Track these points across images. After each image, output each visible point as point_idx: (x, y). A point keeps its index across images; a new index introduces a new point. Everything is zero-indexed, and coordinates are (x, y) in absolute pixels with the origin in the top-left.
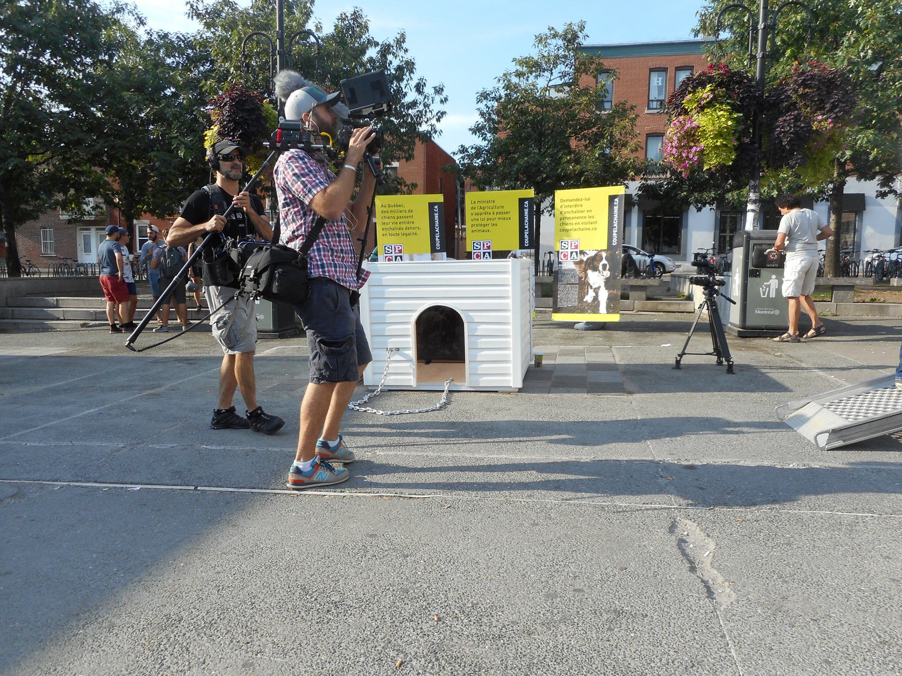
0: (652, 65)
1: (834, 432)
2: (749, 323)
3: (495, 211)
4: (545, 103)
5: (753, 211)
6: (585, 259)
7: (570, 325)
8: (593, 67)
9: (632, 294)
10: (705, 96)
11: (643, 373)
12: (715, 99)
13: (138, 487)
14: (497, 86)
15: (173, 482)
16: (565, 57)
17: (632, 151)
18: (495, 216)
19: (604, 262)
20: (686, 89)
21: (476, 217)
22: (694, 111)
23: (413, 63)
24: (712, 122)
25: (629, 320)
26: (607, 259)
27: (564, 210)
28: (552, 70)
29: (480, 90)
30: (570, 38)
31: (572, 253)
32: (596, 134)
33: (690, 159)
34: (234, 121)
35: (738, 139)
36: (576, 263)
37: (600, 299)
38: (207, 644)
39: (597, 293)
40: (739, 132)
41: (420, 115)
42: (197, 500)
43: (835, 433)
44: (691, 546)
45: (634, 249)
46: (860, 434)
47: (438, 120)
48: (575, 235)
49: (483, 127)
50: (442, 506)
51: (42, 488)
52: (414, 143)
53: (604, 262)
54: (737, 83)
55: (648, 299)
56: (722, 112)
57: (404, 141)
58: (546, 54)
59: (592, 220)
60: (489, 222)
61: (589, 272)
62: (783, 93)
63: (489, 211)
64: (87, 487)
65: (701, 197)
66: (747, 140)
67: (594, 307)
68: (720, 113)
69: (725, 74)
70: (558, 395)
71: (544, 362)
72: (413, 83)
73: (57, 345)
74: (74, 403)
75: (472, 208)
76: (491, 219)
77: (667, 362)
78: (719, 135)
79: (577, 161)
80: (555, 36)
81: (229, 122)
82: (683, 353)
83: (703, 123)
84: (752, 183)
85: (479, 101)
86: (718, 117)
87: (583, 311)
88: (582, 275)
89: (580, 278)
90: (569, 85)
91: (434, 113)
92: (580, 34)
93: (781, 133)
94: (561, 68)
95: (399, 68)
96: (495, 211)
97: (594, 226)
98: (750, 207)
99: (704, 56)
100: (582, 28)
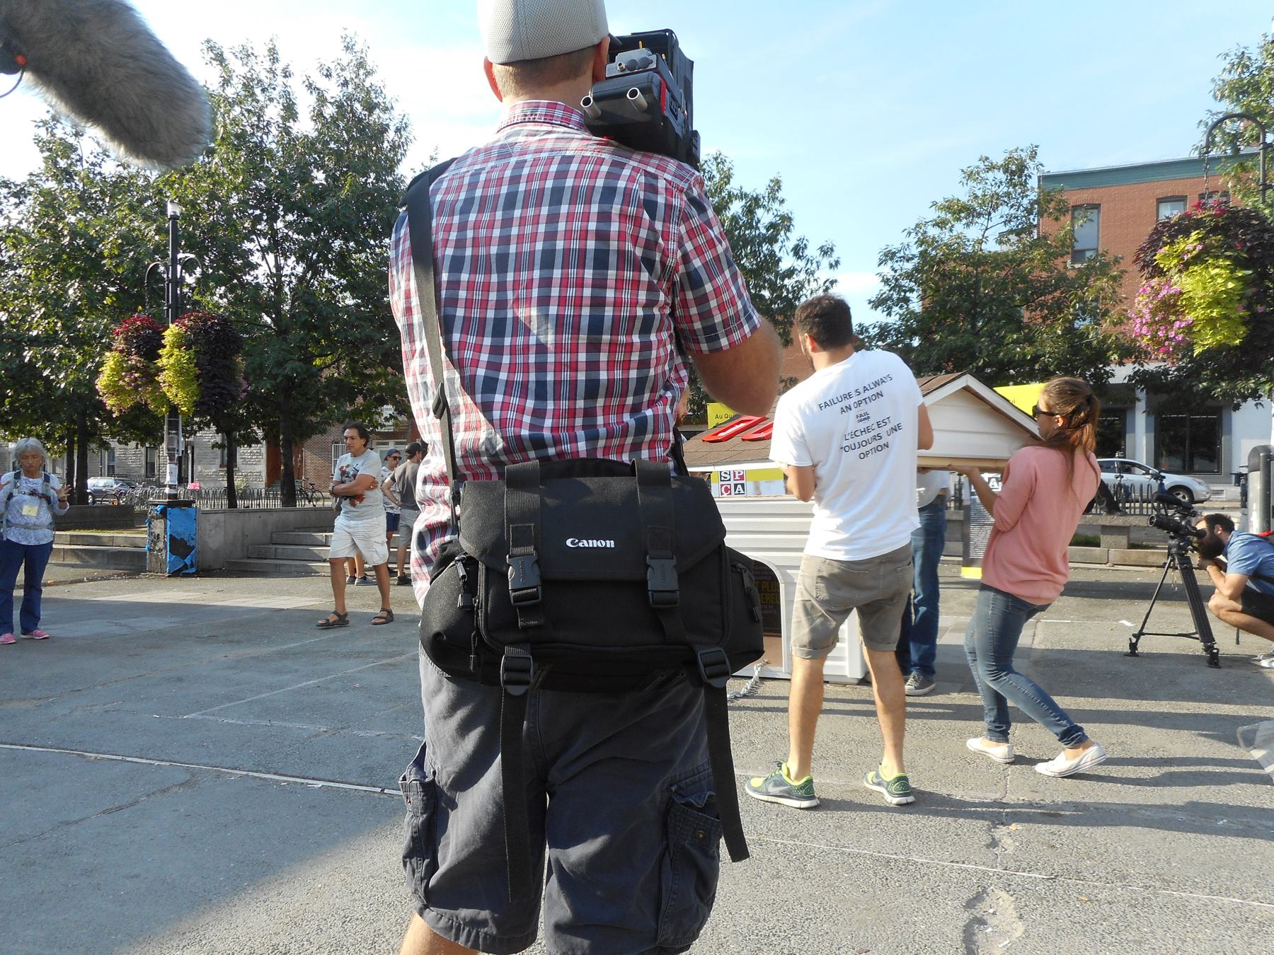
0: (1160, 193)
4: (978, 260)
8: (1052, 205)
9: (1105, 539)
10: (1190, 247)
11: (1066, 664)
12: (1206, 251)
13: (320, 784)
14: (906, 241)
15: (359, 781)
16: (1008, 194)
17: (1115, 324)
20: (1159, 239)
22: (1174, 271)
24: (1204, 285)
25: (1093, 580)
30: (1016, 170)
31: (736, 486)
32: (1059, 298)
33: (1171, 340)
35: (1248, 307)
40: (1254, 293)
41: (800, 286)
42: (375, 806)
44: (989, 930)
45: (1140, 467)
49: (890, 298)
51: (218, 777)
54: (1241, 226)
56: (1217, 270)
58: (979, 193)
64: (265, 779)
65: (1235, 387)
66: (1260, 309)
68: (1214, 272)
72: (790, 245)
73: (313, 594)
74: (297, 671)
77: (1114, 649)
78: (1216, 302)
79: (1030, 340)
80: (992, 168)
82: (1141, 633)
86: (1212, 277)
91: (821, 282)
92: (1031, 164)
94: (1004, 210)
95: (772, 226)
100: (1033, 155)
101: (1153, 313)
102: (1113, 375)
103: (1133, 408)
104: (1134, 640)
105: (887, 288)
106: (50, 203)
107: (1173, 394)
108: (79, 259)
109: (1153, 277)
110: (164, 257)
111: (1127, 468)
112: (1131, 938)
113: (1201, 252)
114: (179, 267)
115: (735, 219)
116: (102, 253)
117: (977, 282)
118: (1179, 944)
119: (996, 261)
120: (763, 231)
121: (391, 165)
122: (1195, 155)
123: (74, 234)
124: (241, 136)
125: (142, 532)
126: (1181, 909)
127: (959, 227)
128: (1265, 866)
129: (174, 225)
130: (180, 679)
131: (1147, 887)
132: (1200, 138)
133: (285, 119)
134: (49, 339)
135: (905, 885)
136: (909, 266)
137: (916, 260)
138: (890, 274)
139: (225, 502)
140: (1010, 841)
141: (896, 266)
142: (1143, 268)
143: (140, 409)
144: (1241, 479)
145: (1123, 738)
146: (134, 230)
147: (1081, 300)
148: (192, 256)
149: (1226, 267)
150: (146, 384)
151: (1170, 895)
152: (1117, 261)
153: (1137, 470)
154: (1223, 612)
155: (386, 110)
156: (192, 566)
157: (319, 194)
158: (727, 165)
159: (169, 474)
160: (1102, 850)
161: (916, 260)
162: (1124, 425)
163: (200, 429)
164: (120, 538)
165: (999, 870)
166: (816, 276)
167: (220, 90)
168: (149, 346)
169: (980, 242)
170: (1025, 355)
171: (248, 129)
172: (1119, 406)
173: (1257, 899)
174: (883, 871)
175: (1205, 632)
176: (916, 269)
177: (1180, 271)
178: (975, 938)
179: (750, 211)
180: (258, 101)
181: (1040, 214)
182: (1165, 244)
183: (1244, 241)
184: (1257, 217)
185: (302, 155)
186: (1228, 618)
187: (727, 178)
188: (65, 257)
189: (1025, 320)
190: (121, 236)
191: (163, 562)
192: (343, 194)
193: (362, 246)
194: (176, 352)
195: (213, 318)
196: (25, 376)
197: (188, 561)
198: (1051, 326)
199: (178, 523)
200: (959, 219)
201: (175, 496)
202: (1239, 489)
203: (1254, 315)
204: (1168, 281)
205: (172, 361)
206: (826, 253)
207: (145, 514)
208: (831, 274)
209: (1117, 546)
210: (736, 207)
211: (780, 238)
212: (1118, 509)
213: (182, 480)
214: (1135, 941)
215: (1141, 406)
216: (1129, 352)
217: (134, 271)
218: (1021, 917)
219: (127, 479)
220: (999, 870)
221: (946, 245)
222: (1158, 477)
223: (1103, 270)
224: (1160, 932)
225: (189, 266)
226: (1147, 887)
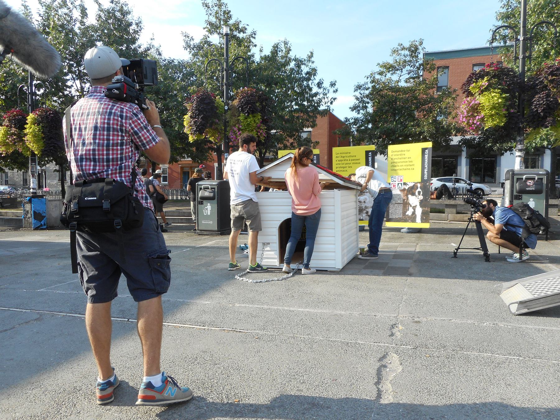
0: (474, 62)
1: (521, 303)
3: (351, 158)
4: (397, 90)
5: (519, 156)
6: (407, 188)
7: (398, 230)
8: (428, 66)
9: (447, 210)
10: (483, 84)
14: (366, 81)
15: (118, 316)
16: (410, 61)
19: (419, 190)
20: (471, 80)
21: (339, 162)
22: (477, 94)
23: (316, 70)
24: (489, 100)
25: (441, 227)
26: (421, 188)
27: (394, 157)
28: (402, 69)
29: (356, 84)
30: (414, 50)
34: (199, 110)
35: (507, 110)
36: (401, 191)
37: (416, 213)
38: (86, 403)
39: (414, 210)
40: (509, 104)
41: (320, 100)
43: (522, 303)
46: (540, 305)
47: (331, 103)
48: (400, 173)
49: (359, 106)
50: (254, 337)
51: (53, 316)
52: (316, 117)
53: (419, 190)
54: (505, 75)
55: (458, 213)
57: (309, 116)
59: (411, 164)
60: (347, 165)
61: (410, 196)
62: (537, 80)
63: (347, 158)
64: (72, 316)
65: (502, 146)
66: (512, 111)
67: (413, 219)
69: (496, 70)
72: (316, 82)
75: (337, 157)
76: (348, 164)
78: (493, 108)
79: (418, 126)
80: (403, 49)
81: (196, 110)
82: (459, 248)
83: (483, 101)
84: (518, 138)
86: (492, 97)
87: (405, 221)
88: (405, 198)
89: (404, 200)
90: (414, 78)
91: (329, 99)
92: (420, 47)
93: (537, 105)
94: (408, 68)
95: (308, 73)
96: (351, 158)
97: (412, 167)
99: (499, 56)
100: (421, 43)
101: (468, 112)
102: (452, 140)
103: (461, 155)
104: (456, 251)
107: (477, 149)
109: (468, 97)
110: (27, 82)
111: (457, 181)
112: (446, 371)
114: (34, 88)
115: (292, 69)
117: (396, 99)
118: (465, 373)
119: (404, 90)
120: (304, 76)
121: (134, 41)
125: (21, 210)
126: (467, 359)
127: (389, 75)
128: (502, 341)
130: (37, 274)
131: (454, 350)
132: (489, 36)
133: (83, 17)
135: (354, 353)
136: (367, 92)
137: (370, 89)
138: (359, 96)
139: (61, 197)
140: (399, 334)
142: (464, 93)
143: (16, 153)
144: (503, 184)
145: (448, 291)
146: (12, 70)
147: (440, 108)
149: (498, 93)
150: (19, 142)
151: (463, 353)
152: (455, 91)
153: (462, 182)
154: (492, 238)
156: (44, 225)
158: (289, 45)
159: (33, 183)
160: (437, 335)
161: (370, 89)
162: (457, 163)
163: (48, 163)
164: (10, 213)
165: (394, 345)
166: (328, 96)
168: (20, 124)
169: (398, 82)
170: (416, 132)
171: (65, 22)
172: (454, 154)
173: (498, 354)
174: (345, 347)
175: (484, 246)
176: (370, 94)
177: (480, 94)
178: (382, 373)
179: (299, 66)
181: (423, 70)
182: (474, 82)
183: (506, 81)
184: (512, 71)
186: (495, 241)
187: (289, 51)
189: (416, 116)
190: (5, 72)
191: (31, 223)
194: (33, 126)
195: (50, 111)
197: (42, 223)
198: (427, 119)
199: (37, 205)
200: (389, 72)
201: (36, 193)
202: (503, 189)
203: (509, 113)
204: (475, 98)
205: (31, 130)
207: (21, 201)
208: (334, 95)
209: (452, 213)
210: (292, 64)
211: (312, 78)
212: (453, 197)
213: (40, 186)
214: (447, 372)
215: (464, 154)
216: (460, 131)
217: (12, 89)
218: (401, 364)
219: (14, 186)
220: (394, 345)
221: (383, 82)
222: (469, 184)
223: (449, 95)
224: (457, 368)
225: (38, 87)
226: (454, 350)
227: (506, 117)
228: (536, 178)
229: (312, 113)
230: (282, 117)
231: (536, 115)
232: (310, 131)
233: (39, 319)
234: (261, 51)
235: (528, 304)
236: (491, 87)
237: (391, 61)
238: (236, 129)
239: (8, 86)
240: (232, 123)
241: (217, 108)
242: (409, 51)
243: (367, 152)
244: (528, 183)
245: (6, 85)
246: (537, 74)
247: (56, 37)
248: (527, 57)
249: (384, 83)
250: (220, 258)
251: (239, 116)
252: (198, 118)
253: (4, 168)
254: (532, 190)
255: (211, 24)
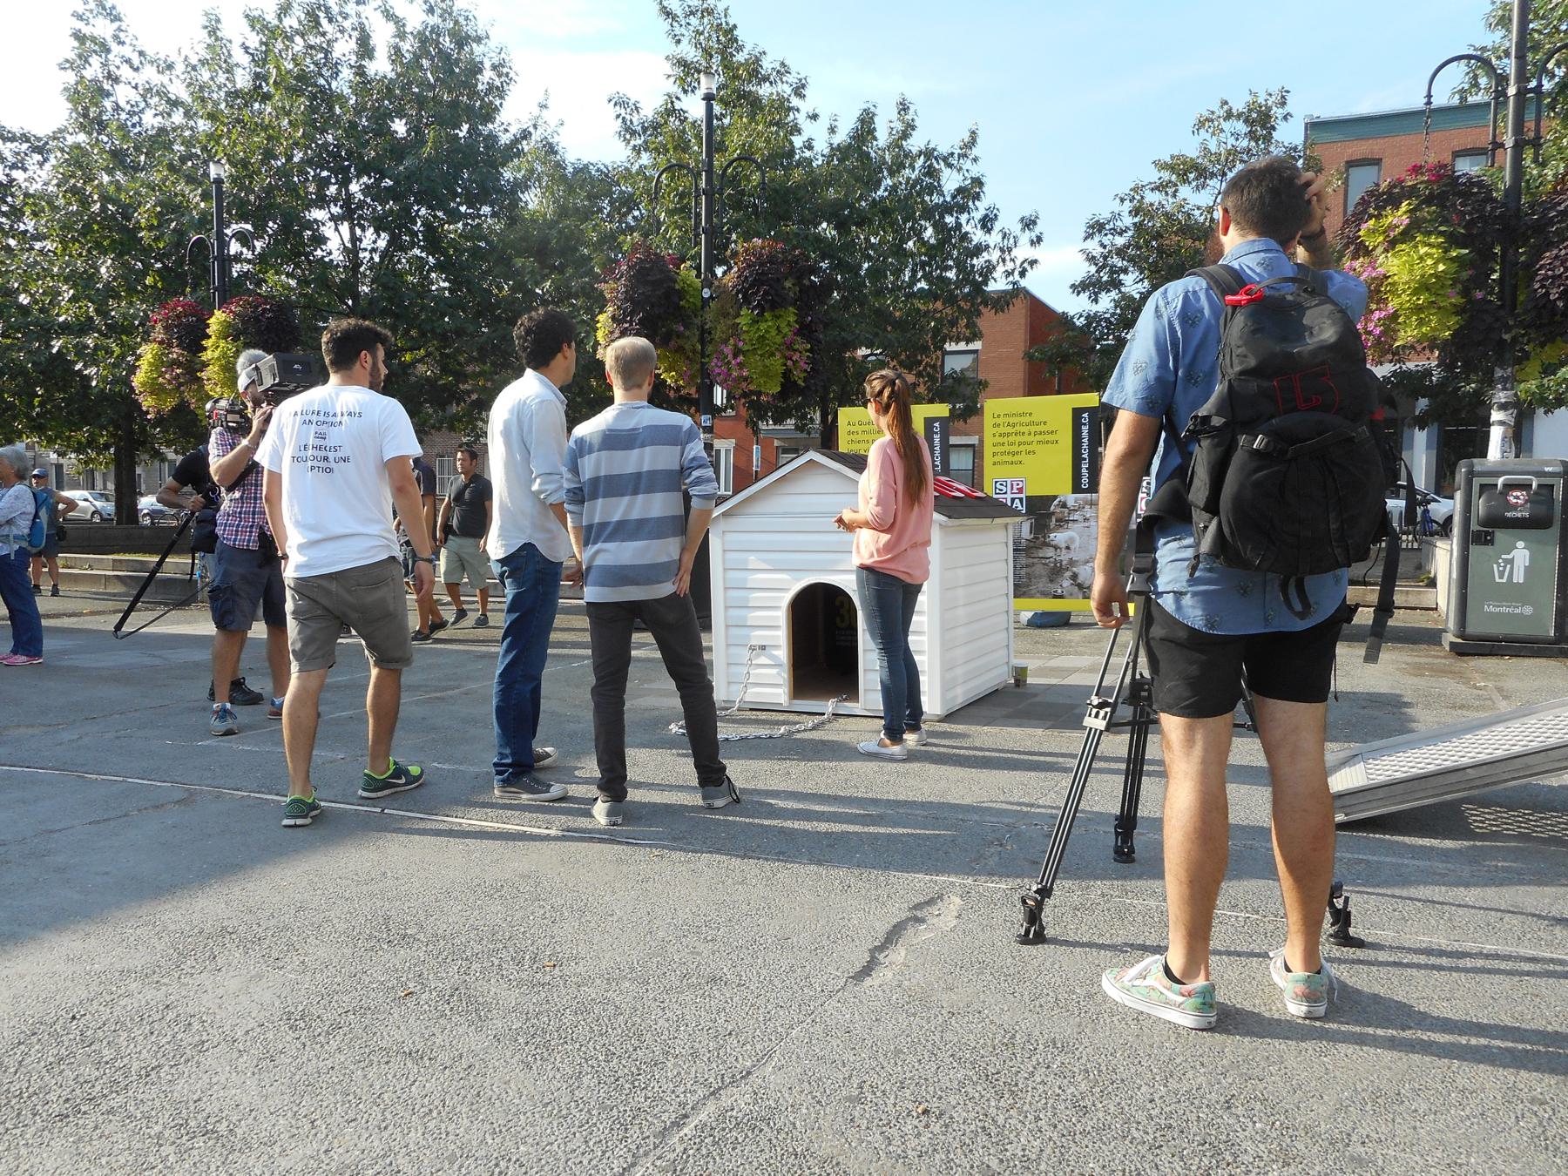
0: (1457, 144)
2: (1471, 629)
3: (1033, 429)
5: (1501, 423)
18: (1031, 438)
20: (1365, 211)
21: (1001, 440)
35: (1465, 292)
40: (1469, 278)
41: (989, 269)
46: (1375, 804)
47: (1023, 274)
52: (979, 314)
54: (1460, 194)
63: (1023, 429)
68: (1423, 250)
70: (1030, 731)
71: (1029, 680)
72: (978, 215)
75: (995, 425)
76: (1025, 443)
78: (1423, 287)
80: (1229, 115)
83: (1395, 270)
85: (1089, 236)
86: (1421, 258)
91: (1018, 263)
93: (1546, 278)
95: (960, 191)
96: (1033, 429)
98: (1496, 416)
105: (1093, 269)
106: (78, 161)
108: (111, 230)
113: (1408, 226)
116: (138, 222)
121: (489, 114)
122: (1456, 101)
123: (105, 199)
124: (303, 77)
127: (1185, 191)
129: (219, 189)
131: (1103, 895)
134: (84, 327)
136: (1120, 241)
141: (1106, 241)
146: (176, 195)
148: (249, 227)
149: (1439, 246)
155: (478, 40)
157: (398, 150)
158: (911, 112)
161: (1130, 233)
167: (276, 22)
176: (1126, 246)
177: (1386, 251)
180: (324, 34)
182: (1371, 217)
185: (380, 100)
187: (908, 129)
188: (96, 227)
192: (427, 150)
193: (454, 216)
194: (222, 343)
196: (57, 371)
200: (1186, 181)
205: (216, 354)
206: (1027, 225)
208: (1031, 253)
227: (1457, 314)
228: (1534, 486)
229: (969, 301)
230: (882, 316)
231: (1544, 306)
232: (975, 352)
233: (188, 801)
234: (832, 130)
235: (1347, 801)
236: (1419, 229)
237: (1192, 151)
238: (728, 350)
239: (166, 238)
240: (718, 335)
241: (681, 294)
242: (1246, 121)
243: (1077, 413)
244: (1512, 500)
245: (163, 234)
246: (1555, 191)
247: (283, 108)
248: (1528, 142)
249: (1167, 215)
250: (655, 686)
251: (738, 315)
252: (631, 322)
253: (164, 449)
254: (1523, 519)
255: (683, 64)
